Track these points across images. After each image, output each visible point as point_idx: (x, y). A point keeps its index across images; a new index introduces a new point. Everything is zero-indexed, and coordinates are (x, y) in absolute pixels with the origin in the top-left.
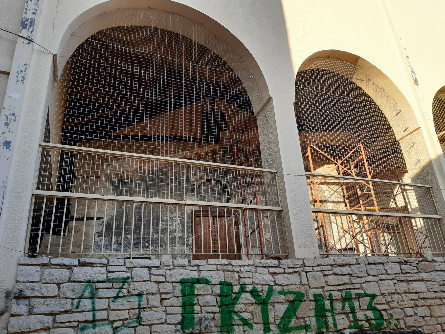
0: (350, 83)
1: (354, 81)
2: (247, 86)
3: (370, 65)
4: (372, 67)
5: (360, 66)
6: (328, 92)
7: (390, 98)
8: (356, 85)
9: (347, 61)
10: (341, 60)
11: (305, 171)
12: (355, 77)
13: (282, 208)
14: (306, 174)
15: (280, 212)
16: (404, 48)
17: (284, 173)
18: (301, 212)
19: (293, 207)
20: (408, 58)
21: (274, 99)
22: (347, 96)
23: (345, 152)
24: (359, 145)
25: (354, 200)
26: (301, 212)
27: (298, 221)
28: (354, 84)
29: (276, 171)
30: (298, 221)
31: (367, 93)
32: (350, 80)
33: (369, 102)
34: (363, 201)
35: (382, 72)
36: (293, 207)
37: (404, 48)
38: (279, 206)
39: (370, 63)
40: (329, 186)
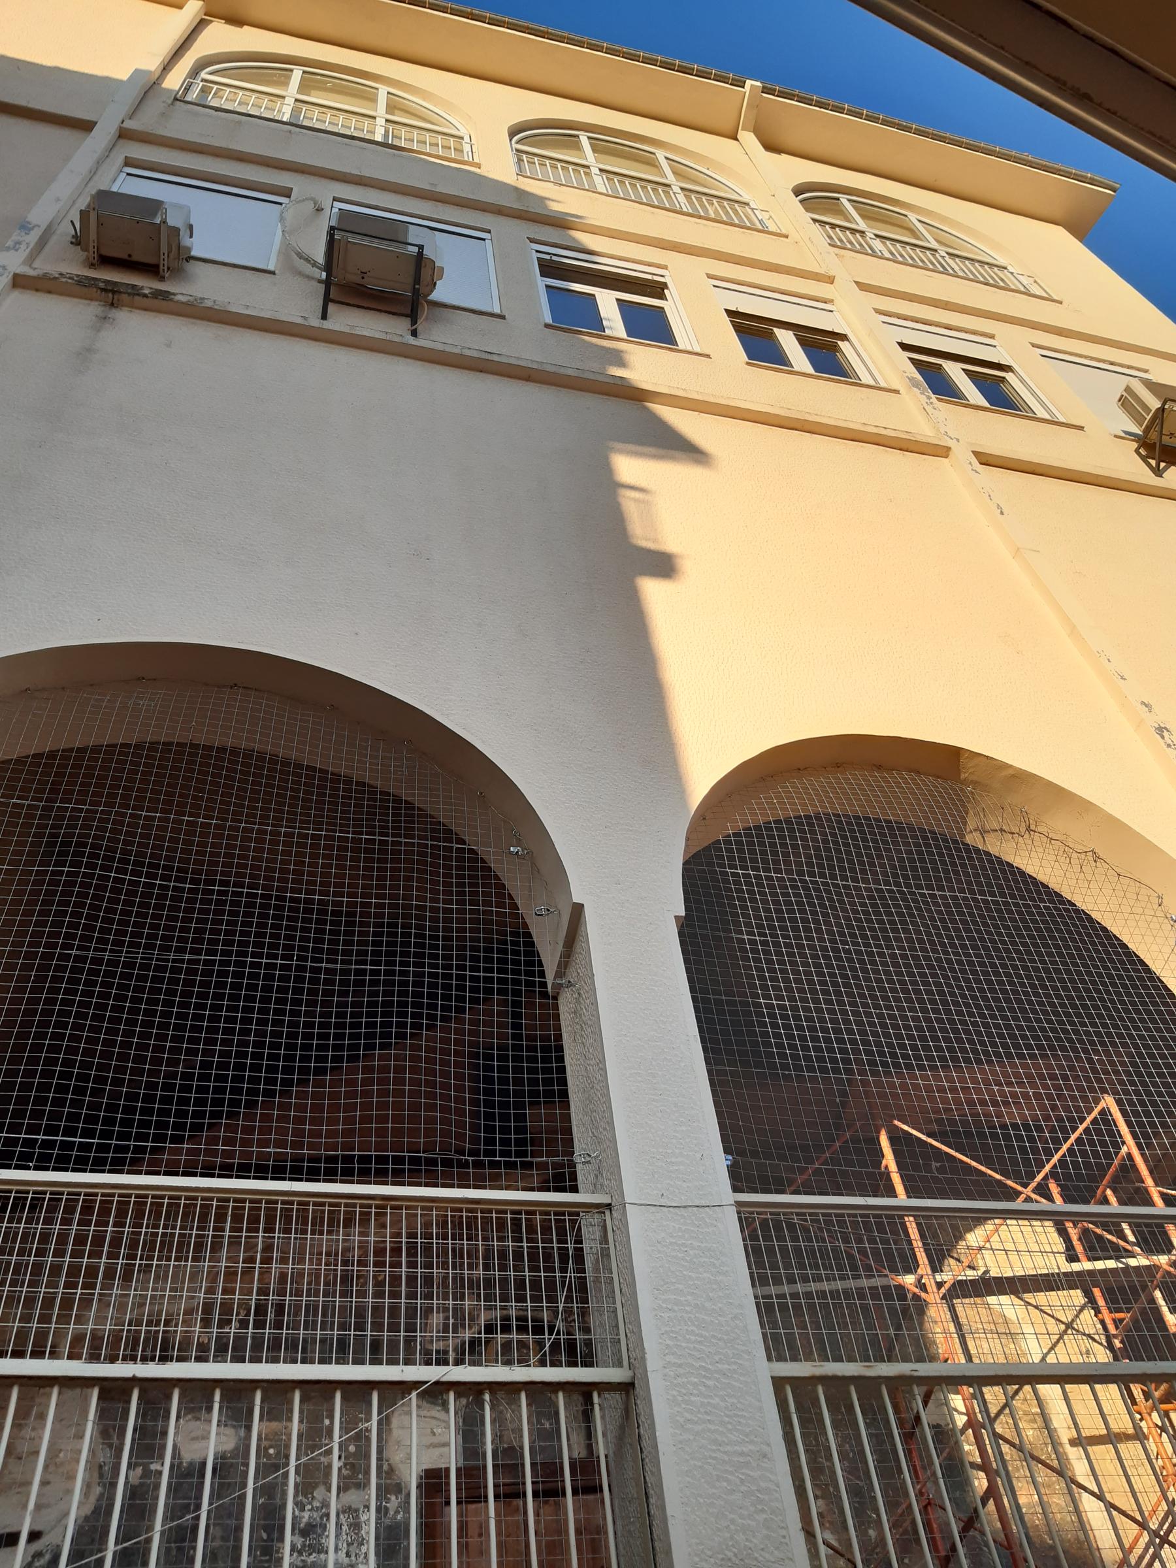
0: (958, 850)
1: (973, 839)
2: (516, 888)
3: (1011, 772)
4: (1019, 779)
5: (975, 783)
6: (844, 878)
7: (1132, 883)
8: (988, 854)
9: (918, 773)
10: (890, 770)
11: (736, 1189)
12: (971, 823)
13: (630, 1373)
14: (739, 1204)
15: (627, 1388)
16: (1143, 703)
17: (627, 1200)
18: (710, 1383)
19: (670, 1358)
20: (1166, 734)
21: (588, 912)
22: (930, 887)
23: (1084, 1154)
24: (1102, 1104)
25: (784, 1250)
26: (710, 1383)
27: (698, 1428)
28: (977, 851)
29: (605, 1199)
30: (698, 1428)
31: (1042, 877)
32: (955, 842)
33: (1032, 899)
34: (910, 1266)
35: (1063, 789)
36: (670, 1358)
37: (1143, 703)
38: (620, 1364)
39: (1006, 766)
40: (1028, 1297)
